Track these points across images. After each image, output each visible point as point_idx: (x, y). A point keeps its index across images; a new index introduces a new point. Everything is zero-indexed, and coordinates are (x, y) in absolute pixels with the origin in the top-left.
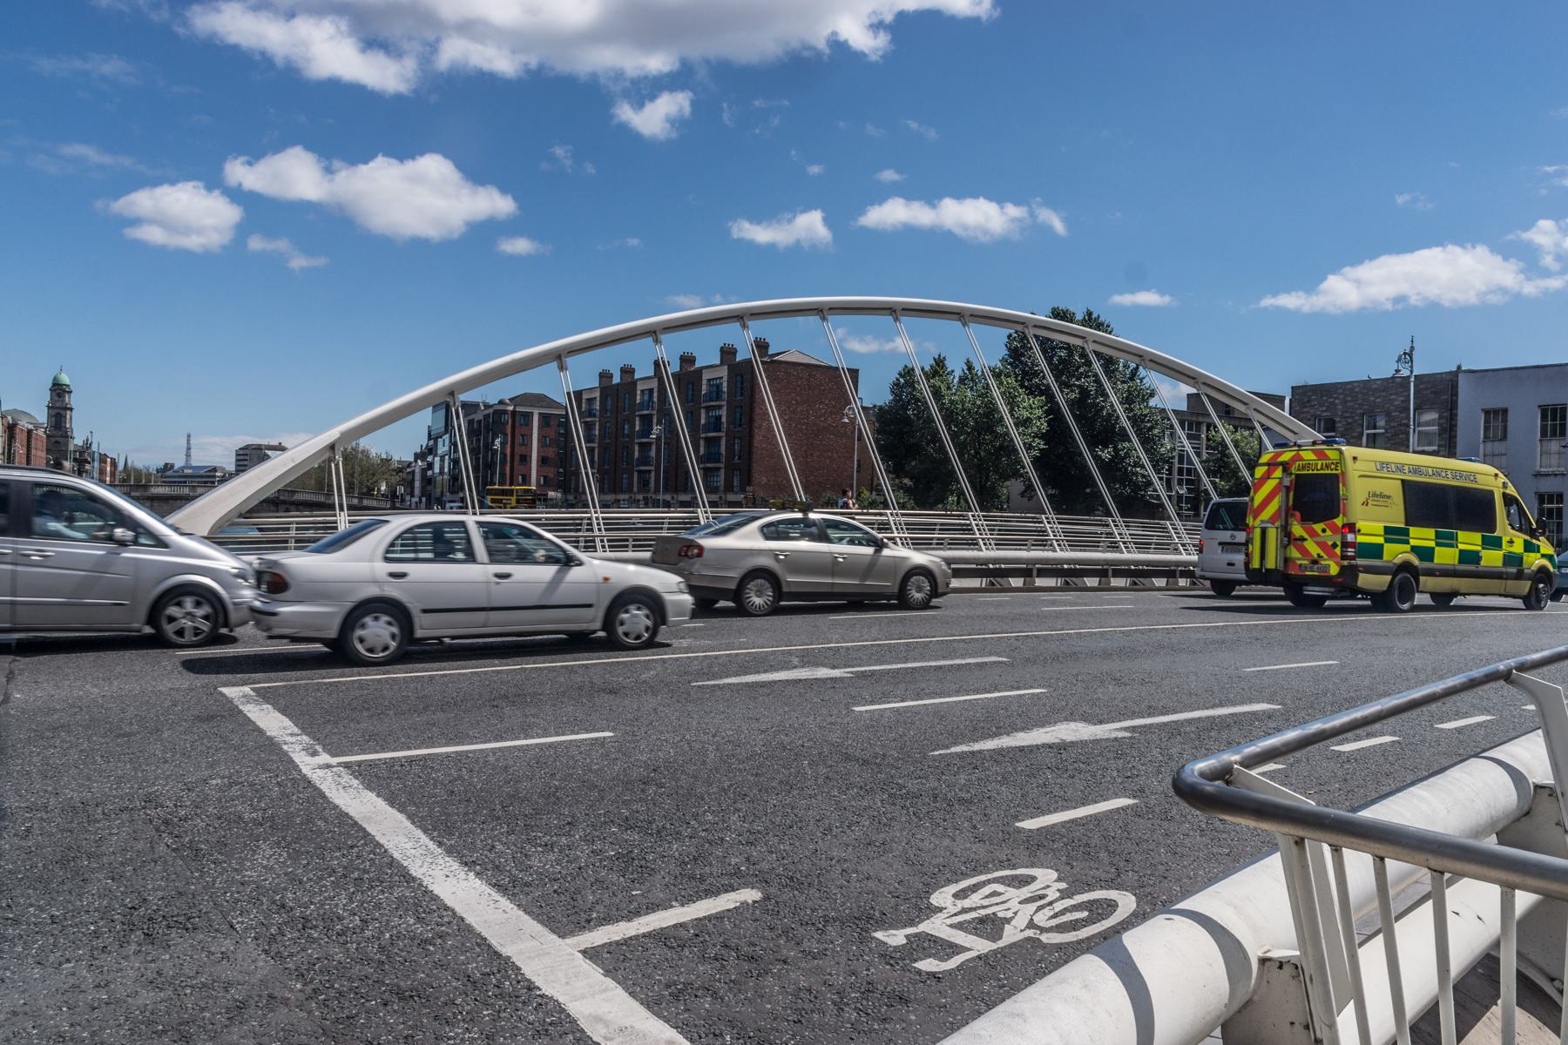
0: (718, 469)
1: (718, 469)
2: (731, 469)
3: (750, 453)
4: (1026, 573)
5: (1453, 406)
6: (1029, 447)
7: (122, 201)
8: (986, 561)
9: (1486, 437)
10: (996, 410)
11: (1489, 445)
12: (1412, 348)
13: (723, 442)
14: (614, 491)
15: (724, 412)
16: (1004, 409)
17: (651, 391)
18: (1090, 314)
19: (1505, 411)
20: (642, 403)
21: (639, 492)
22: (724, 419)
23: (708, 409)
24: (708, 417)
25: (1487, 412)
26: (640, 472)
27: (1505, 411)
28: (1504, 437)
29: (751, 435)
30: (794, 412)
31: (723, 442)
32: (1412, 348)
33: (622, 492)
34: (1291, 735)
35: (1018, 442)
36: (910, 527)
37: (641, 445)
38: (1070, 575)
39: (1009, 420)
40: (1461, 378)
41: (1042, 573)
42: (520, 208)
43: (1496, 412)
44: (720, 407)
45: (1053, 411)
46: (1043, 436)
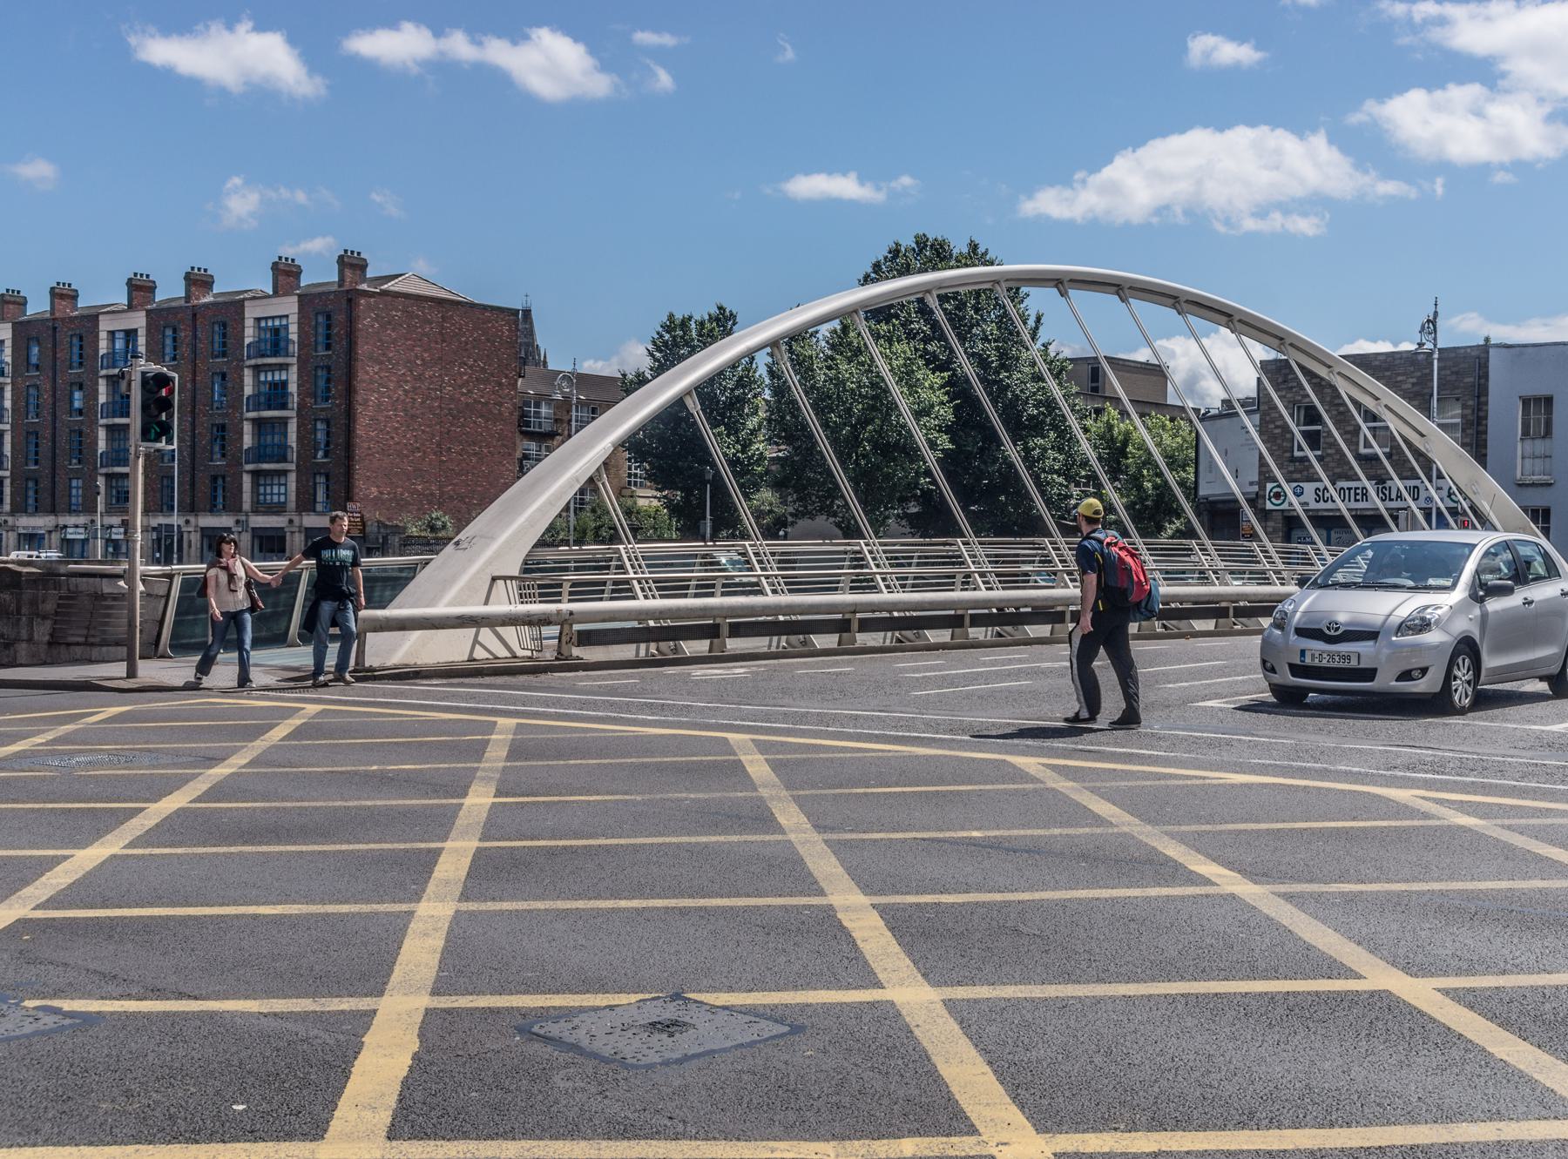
0: (285, 473)
1: (285, 473)
2: (307, 471)
3: (349, 447)
4: (842, 627)
5: (1481, 392)
6: (932, 445)
7: (1370, 106)
8: (641, 615)
9: (1526, 433)
10: (886, 391)
11: (1528, 443)
12: (1436, 313)
13: (292, 428)
14: (53, 511)
15: (292, 378)
16: (896, 391)
17: (130, 334)
18: (974, 247)
19: (1549, 401)
20: (112, 354)
21: (109, 511)
22: (293, 388)
23: (257, 369)
24: (257, 383)
25: (1526, 402)
26: (108, 476)
27: (1549, 401)
28: (1548, 433)
29: (350, 414)
30: (419, 378)
31: (292, 428)
32: (1436, 313)
33: (70, 511)
34: (1549, 821)
35: (920, 438)
36: (653, 562)
37: (110, 429)
38: (906, 626)
39: (904, 405)
40: (1492, 351)
41: (865, 626)
42: (279, 29)
43: (1537, 400)
44: (284, 367)
45: (958, 389)
46: (948, 430)
